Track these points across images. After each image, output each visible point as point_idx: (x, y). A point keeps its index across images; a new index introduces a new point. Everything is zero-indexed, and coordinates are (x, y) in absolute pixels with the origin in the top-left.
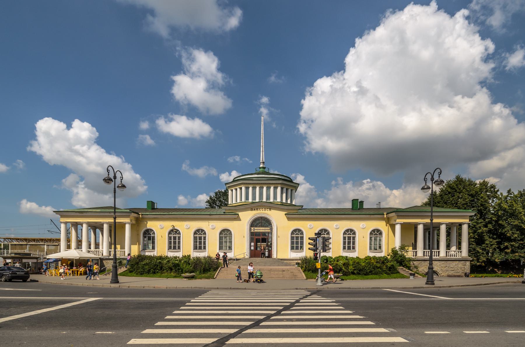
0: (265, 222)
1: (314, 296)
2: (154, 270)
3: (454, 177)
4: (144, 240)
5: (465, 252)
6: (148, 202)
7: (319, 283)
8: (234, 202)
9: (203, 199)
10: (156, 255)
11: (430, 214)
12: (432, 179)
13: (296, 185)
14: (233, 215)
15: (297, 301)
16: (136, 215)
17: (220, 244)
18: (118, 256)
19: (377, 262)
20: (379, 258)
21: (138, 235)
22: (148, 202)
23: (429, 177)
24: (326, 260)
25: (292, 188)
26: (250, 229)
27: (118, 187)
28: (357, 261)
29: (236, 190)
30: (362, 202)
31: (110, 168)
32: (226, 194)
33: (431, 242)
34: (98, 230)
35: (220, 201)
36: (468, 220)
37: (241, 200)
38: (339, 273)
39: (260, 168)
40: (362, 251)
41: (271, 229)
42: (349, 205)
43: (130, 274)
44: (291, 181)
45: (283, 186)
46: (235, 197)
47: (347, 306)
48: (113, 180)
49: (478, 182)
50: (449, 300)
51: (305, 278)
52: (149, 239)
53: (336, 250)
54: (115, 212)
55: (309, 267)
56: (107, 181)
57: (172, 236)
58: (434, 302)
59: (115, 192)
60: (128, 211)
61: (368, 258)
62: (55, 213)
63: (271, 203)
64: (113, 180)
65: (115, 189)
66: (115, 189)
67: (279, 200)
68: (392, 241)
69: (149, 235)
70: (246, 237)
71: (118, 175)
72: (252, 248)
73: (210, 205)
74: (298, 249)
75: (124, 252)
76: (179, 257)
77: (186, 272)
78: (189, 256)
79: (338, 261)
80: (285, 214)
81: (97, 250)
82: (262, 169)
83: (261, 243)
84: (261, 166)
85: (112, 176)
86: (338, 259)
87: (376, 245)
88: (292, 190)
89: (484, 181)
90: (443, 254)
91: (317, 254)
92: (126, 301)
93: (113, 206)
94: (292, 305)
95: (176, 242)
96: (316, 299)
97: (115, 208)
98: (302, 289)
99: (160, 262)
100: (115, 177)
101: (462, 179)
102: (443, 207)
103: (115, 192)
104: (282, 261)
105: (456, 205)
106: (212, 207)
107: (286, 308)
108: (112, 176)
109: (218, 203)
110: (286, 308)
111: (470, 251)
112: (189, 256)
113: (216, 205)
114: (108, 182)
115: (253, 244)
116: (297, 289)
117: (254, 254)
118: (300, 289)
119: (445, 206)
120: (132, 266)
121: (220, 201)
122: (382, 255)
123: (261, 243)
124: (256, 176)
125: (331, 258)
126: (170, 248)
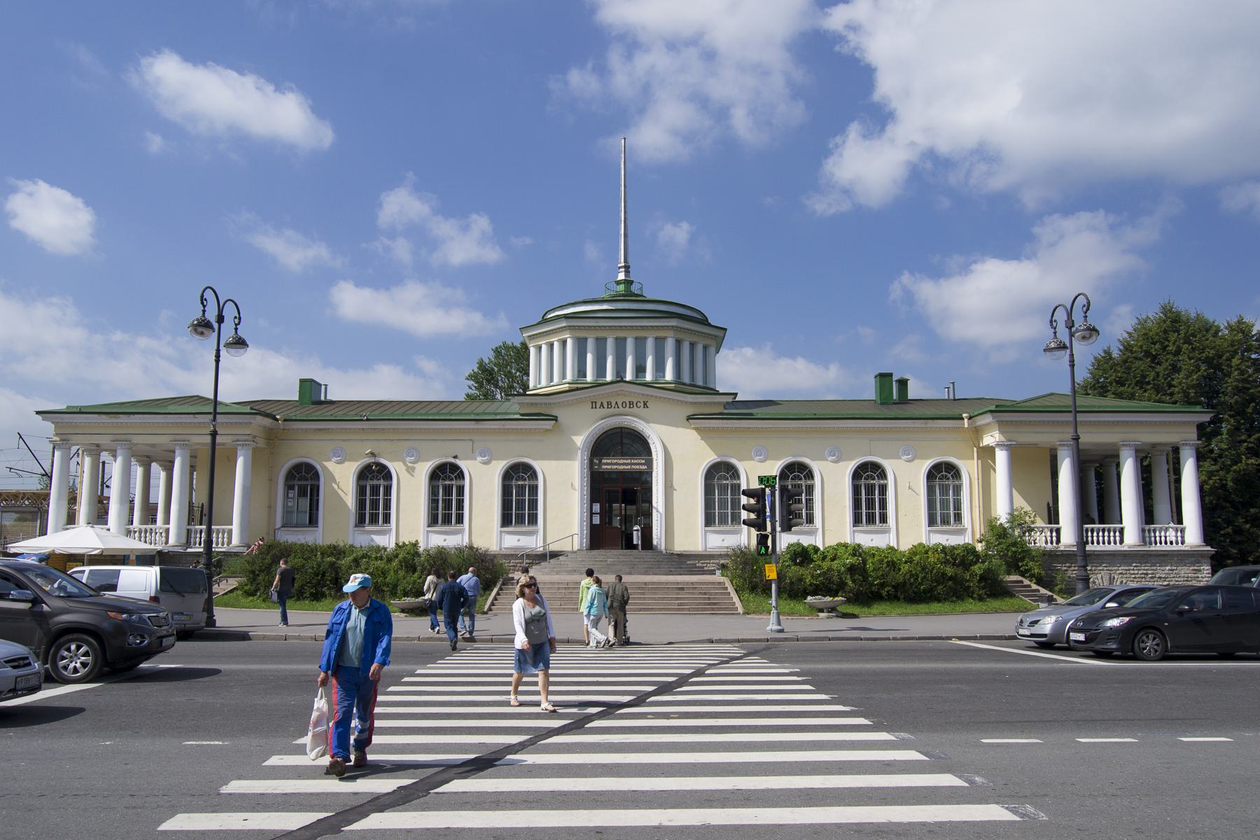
0: (635, 443)
1: (754, 660)
2: (315, 586)
3: (1157, 309)
4: (286, 497)
5: (1192, 534)
6: (302, 381)
7: (772, 626)
8: (544, 383)
9: (450, 385)
10: (320, 542)
11: (1069, 417)
12: (1070, 325)
13: (720, 333)
14: (543, 414)
15: (699, 672)
16: (268, 422)
17: (706, 494)
18: (218, 548)
19: (946, 562)
20: (953, 548)
21: (272, 480)
22: (302, 381)
23: (1061, 316)
24: (802, 555)
25: (708, 342)
26: (591, 464)
27: (228, 345)
28: (890, 559)
29: (551, 345)
30: (903, 383)
31: (209, 295)
32: (521, 355)
33: (1098, 504)
34: (155, 466)
35: (509, 375)
36: (1195, 436)
37: (564, 376)
38: (836, 595)
39: (618, 283)
40: (907, 528)
41: (650, 463)
42: (869, 391)
43: (244, 601)
44: (704, 321)
45: (680, 336)
46: (549, 370)
47: (820, 682)
48: (216, 326)
49: (1222, 324)
50: (1101, 668)
51: (740, 610)
52: (302, 493)
53: (832, 525)
54: (215, 413)
55: (749, 574)
56: (200, 329)
57: (369, 484)
58: (1062, 672)
59: (217, 361)
60: (247, 409)
61: (921, 551)
62: (39, 417)
63: (646, 385)
64: (216, 326)
65: (218, 351)
66: (218, 351)
67: (669, 375)
68: (994, 496)
69: (305, 482)
70: (577, 484)
71: (230, 312)
72: (597, 520)
73: (481, 386)
74: (948, 523)
75: (230, 532)
76: (385, 549)
77: (406, 594)
78: (415, 545)
79: (833, 560)
80: (689, 418)
81: (149, 527)
82: (621, 288)
83: (620, 501)
84: (621, 276)
85: (212, 316)
86: (833, 554)
87: (942, 508)
88: (705, 348)
89: (1240, 322)
90: (1131, 538)
91: (767, 537)
92: (243, 671)
93: (212, 397)
94: (683, 680)
95: (873, 500)
96: (756, 665)
97: (215, 402)
98: (727, 641)
99: (332, 565)
100: (221, 319)
101: (1178, 314)
102: (1131, 397)
103: (217, 361)
104: (684, 562)
105: (1162, 391)
106: (488, 396)
107: (664, 689)
108: (212, 316)
109: (503, 381)
110: (664, 689)
111: (1210, 529)
112: (415, 545)
113: (496, 386)
114: (202, 333)
115: (597, 507)
116: (712, 642)
117: (598, 537)
118: (720, 641)
119: (1139, 392)
120: (253, 576)
121: (509, 375)
122: (966, 539)
123: (620, 501)
124: (605, 307)
125: (816, 550)
126: (433, 521)
